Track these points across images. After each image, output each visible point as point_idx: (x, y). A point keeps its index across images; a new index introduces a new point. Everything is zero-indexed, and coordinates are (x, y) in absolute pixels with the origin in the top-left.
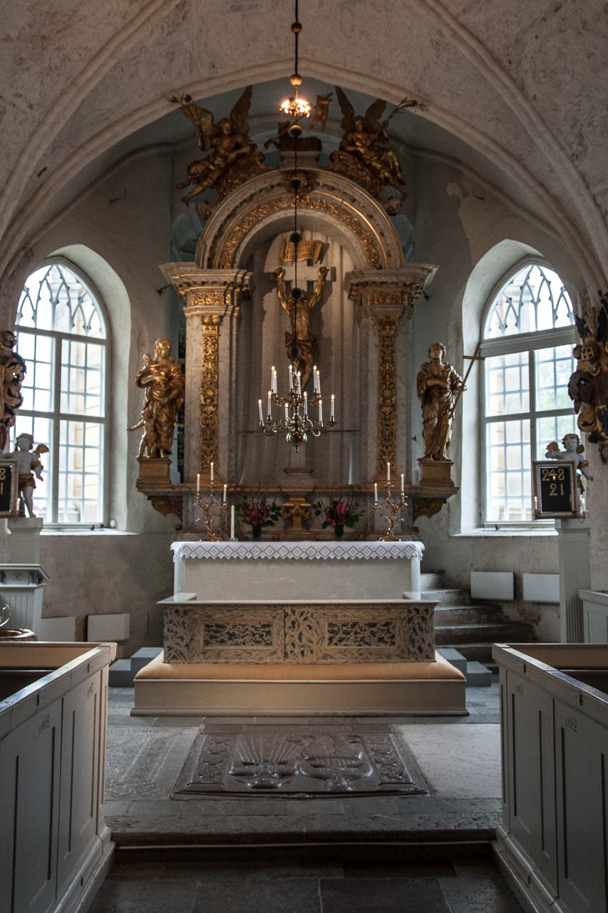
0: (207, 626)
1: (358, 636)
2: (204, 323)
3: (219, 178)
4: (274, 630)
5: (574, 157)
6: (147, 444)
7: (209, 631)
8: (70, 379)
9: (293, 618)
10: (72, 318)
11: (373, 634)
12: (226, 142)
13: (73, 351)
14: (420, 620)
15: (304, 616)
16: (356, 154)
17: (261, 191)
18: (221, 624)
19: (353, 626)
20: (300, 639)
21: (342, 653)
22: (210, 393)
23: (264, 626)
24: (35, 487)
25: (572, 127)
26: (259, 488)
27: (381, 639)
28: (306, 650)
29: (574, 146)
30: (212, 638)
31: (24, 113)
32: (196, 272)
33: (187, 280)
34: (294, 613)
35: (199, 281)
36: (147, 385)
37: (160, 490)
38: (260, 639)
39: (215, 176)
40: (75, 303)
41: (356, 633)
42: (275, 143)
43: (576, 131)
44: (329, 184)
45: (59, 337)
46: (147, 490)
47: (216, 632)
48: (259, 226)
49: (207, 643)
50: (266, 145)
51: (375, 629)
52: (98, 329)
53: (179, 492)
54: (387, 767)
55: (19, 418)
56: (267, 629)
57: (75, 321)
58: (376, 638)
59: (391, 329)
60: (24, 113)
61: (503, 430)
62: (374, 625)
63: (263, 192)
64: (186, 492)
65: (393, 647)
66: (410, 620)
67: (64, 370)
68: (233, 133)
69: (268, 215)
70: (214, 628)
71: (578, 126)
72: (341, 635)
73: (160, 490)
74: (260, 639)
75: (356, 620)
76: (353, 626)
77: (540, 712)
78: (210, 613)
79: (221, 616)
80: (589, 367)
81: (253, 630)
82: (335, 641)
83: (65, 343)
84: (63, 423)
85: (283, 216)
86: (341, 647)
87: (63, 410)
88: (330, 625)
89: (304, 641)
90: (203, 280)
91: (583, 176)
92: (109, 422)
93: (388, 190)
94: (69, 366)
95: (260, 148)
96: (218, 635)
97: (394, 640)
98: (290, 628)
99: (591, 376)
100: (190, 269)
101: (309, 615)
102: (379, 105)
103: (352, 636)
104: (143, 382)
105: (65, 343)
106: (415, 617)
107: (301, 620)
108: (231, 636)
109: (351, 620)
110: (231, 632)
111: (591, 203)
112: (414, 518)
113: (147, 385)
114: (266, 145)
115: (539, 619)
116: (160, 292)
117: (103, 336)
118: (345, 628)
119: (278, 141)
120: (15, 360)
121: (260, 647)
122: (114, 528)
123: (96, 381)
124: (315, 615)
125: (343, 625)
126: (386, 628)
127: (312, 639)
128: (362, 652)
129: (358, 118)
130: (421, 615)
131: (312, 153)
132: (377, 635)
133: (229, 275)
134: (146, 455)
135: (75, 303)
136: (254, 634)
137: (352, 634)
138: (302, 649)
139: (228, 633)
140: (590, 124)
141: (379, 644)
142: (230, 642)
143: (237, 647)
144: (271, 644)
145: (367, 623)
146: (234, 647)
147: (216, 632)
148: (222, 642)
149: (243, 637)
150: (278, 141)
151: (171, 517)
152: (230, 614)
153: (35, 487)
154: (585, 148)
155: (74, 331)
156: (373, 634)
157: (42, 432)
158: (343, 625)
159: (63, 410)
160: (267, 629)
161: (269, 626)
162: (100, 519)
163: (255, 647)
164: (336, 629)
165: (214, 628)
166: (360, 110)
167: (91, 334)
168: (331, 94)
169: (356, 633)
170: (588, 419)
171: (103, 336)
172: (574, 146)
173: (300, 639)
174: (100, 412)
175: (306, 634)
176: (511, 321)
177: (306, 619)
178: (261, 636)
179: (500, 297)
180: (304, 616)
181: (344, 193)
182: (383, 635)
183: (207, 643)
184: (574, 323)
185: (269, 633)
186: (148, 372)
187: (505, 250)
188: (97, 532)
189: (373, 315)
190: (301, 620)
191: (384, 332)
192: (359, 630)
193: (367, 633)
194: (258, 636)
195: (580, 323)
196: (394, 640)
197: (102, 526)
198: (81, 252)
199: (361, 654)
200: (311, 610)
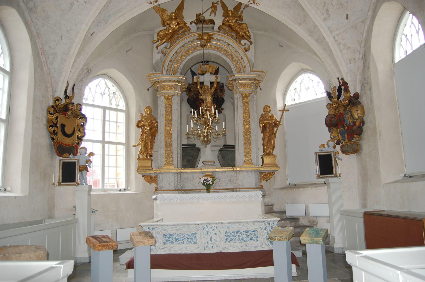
0: (164, 235)
1: (240, 237)
2: (165, 99)
3: (170, 38)
4: (198, 236)
6: (141, 152)
7: (166, 237)
9: (207, 230)
10: (111, 101)
11: (248, 236)
14: (270, 228)
15: (213, 228)
16: (230, 26)
17: (189, 42)
18: (171, 234)
19: (237, 232)
20: (211, 240)
21: (232, 246)
22: (168, 128)
23: (193, 234)
24: (88, 171)
25: (323, 6)
27: (251, 239)
28: (214, 245)
29: (325, 15)
30: (167, 241)
31: (83, 5)
32: (162, 77)
33: (157, 80)
34: (207, 227)
35: (163, 80)
36: (141, 126)
37: (148, 172)
38: (191, 241)
39: (169, 36)
41: (239, 236)
42: (194, 22)
43: (325, 8)
44: (218, 38)
45: (104, 109)
46: (142, 172)
47: (169, 238)
48: (189, 58)
49: (164, 244)
50: (191, 23)
51: (248, 234)
52: (122, 106)
53: (156, 173)
54: (181, 31)
56: (194, 236)
57: (112, 102)
58: (249, 238)
59: (247, 99)
60: (83, 5)
62: (248, 232)
63: (190, 42)
64: (159, 173)
65: (257, 242)
66: (266, 228)
67: (107, 123)
68: (176, 19)
69: (192, 53)
70: (168, 236)
71: (326, 6)
72: (231, 237)
73: (148, 172)
74: (191, 241)
75: (238, 229)
76: (237, 232)
78: (166, 229)
79: (171, 230)
81: (188, 236)
82: (228, 240)
83: (107, 111)
84: (106, 146)
85: (199, 53)
86: (232, 243)
87: (107, 139)
88: (226, 232)
89: (213, 241)
90: (165, 80)
91: (329, 28)
92: (127, 144)
93: (243, 42)
94: (109, 121)
96: (170, 239)
97: (258, 239)
98: (206, 234)
99: (336, 116)
100: (158, 75)
101: (215, 228)
103: (237, 238)
104: (140, 125)
105: (107, 111)
106: (268, 227)
107: (211, 230)
108: (177, 240)
109: (236, 229)
110: (177, 237)
111: (333, 39)
112: (261, 182)
113: (141, 126)
114: (191, 23)
115: (317, 224)
116: (148, 90)
117: (124, 108)
118: (233, 234)
119: (196, 21)
120: (82, 116)
121: (191, 245)
122: (130, 190)
123: (122, 129)
124: (218, 228)
125: (232, 232)
126: (254, 233)
127: (217, 240)
128: (242, 245)
129: (230, 11)
130: (271, 226)
131: (211, 25)
132: (250, 237)
133: (175, 77)
134: (141, 157)
135: (112, 95)
136: (188, 238)
137: (237, 236)
138: (212, 245)
139: (175, 238)
140: (331, 4)
141: (251, 241)
142: (176, 243)
143: (179, 245)
144: (196, 243)
145: (244, 231)
146: (178, 245)
147: (169, 238)
148: (172, 242)
149: (183, 240)
150: (196, 21)
151: (154, 185)
152: (176, 228)
153: (88, 171)
154: (330, 15)
155: (111, 106)
156: (248, 236)
157: (96, 148)
158: (232, 232)
159: (107, 139)
160: (194, 236)
161: (195, 234)
162: (123, 186)
163: (189, 245)
164: (229, 234)
165: (168, 236)
166: (231, 8)
167: (119, 108)
168: (218, 1)
169: (239, 236)
171: (124, 108)
172: (325, 15)
173: (211, 240)
174: (122, 139)
175: (214, 237)
176: (296, 97)
177: (214, 230)
178: (191, 239)
179: (291, 88)
180: (213, 228)
181: (225, 42)
182: (252, 237)
183: (164, 244)
185: (195, 237)
186: (141, 121)
189: (239, 93)
190: (211, 230)
191: (244, 101)
192: (240, 235)
193: (245, 236)
194: (190, 239)
196: (258, 239)
197: (125, 189)
199: (242, 247)
200: (216, 225)
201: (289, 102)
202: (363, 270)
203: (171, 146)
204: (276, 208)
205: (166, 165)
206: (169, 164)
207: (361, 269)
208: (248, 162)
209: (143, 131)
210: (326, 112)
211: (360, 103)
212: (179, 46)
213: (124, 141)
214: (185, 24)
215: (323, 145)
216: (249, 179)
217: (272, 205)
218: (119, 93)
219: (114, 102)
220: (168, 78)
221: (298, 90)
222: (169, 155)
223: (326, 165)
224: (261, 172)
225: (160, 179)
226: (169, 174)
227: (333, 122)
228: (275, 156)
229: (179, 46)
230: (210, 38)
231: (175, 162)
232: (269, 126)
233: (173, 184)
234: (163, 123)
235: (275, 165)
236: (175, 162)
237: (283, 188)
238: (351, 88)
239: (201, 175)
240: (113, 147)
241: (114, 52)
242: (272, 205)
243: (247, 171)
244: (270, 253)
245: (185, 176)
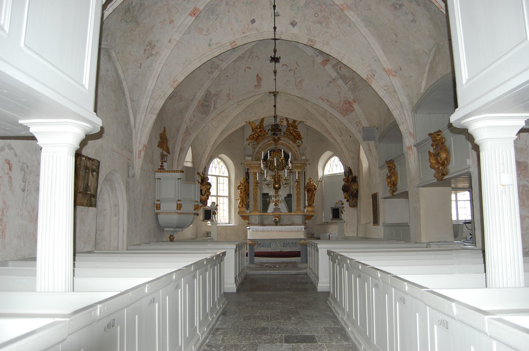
5: (340, 136)
8: (220, 187)
12: (259, 130)
13: (221, 179)
26: (334, 80)
40: (220, 167)
45: (217, 176)
55: (210, 197)
61: (77, 255)
68: (260, 128)
77: (165, 128)
80: (346, 183)
92: (229, 197)
93: (297, 141)
95: (267, 131)
102: (295, 121)
117: (227, 175)
135: (220, 167)
162: (227, 222)
166: (291, 122)
170: (346, 196)
176: (331, 170)
184: (343, 171)
187: (328, 153)
188: (227, 225)
195: (344, 172)
198: (223, 156)
201: (326, 173)
202: (429, 306)
203: (257, 201)
204: (315, 236)
205: (254, 211)
206: (256, 210)
207: (491, 337)
208: (298, 210)
209: (241, 191)
210: (343, 183)
211: (357, 182)
212: (261, 144)
213: (227, 195)
214: (265, 131)
215: (337, 203)
216: (299, 219)
217: (313, 234)
218: (224, 166)
219: (221, 172)
220: (256, 162)
221: (332, 165)
222: (255, 205)
223: (336, 213)
224: (305, 215)
225: (250, 218)
226: (255, 216)
227: (345, 189)
228: (314, 207)
229: (261, 144)
230: (279, 139)
231: (259, 210)
232: (310, 190)
233: (258, 221)
234: (253, 187)
235: (314, 212)
236: (259, 210)
237: (319, 225)
238: (353, 172)
239: (273, 217)
240: (222, 198)
241: (227, 147)
242: (313, 234)
243: (298, 215)
244: (299, 252)
245: (264, 217)
